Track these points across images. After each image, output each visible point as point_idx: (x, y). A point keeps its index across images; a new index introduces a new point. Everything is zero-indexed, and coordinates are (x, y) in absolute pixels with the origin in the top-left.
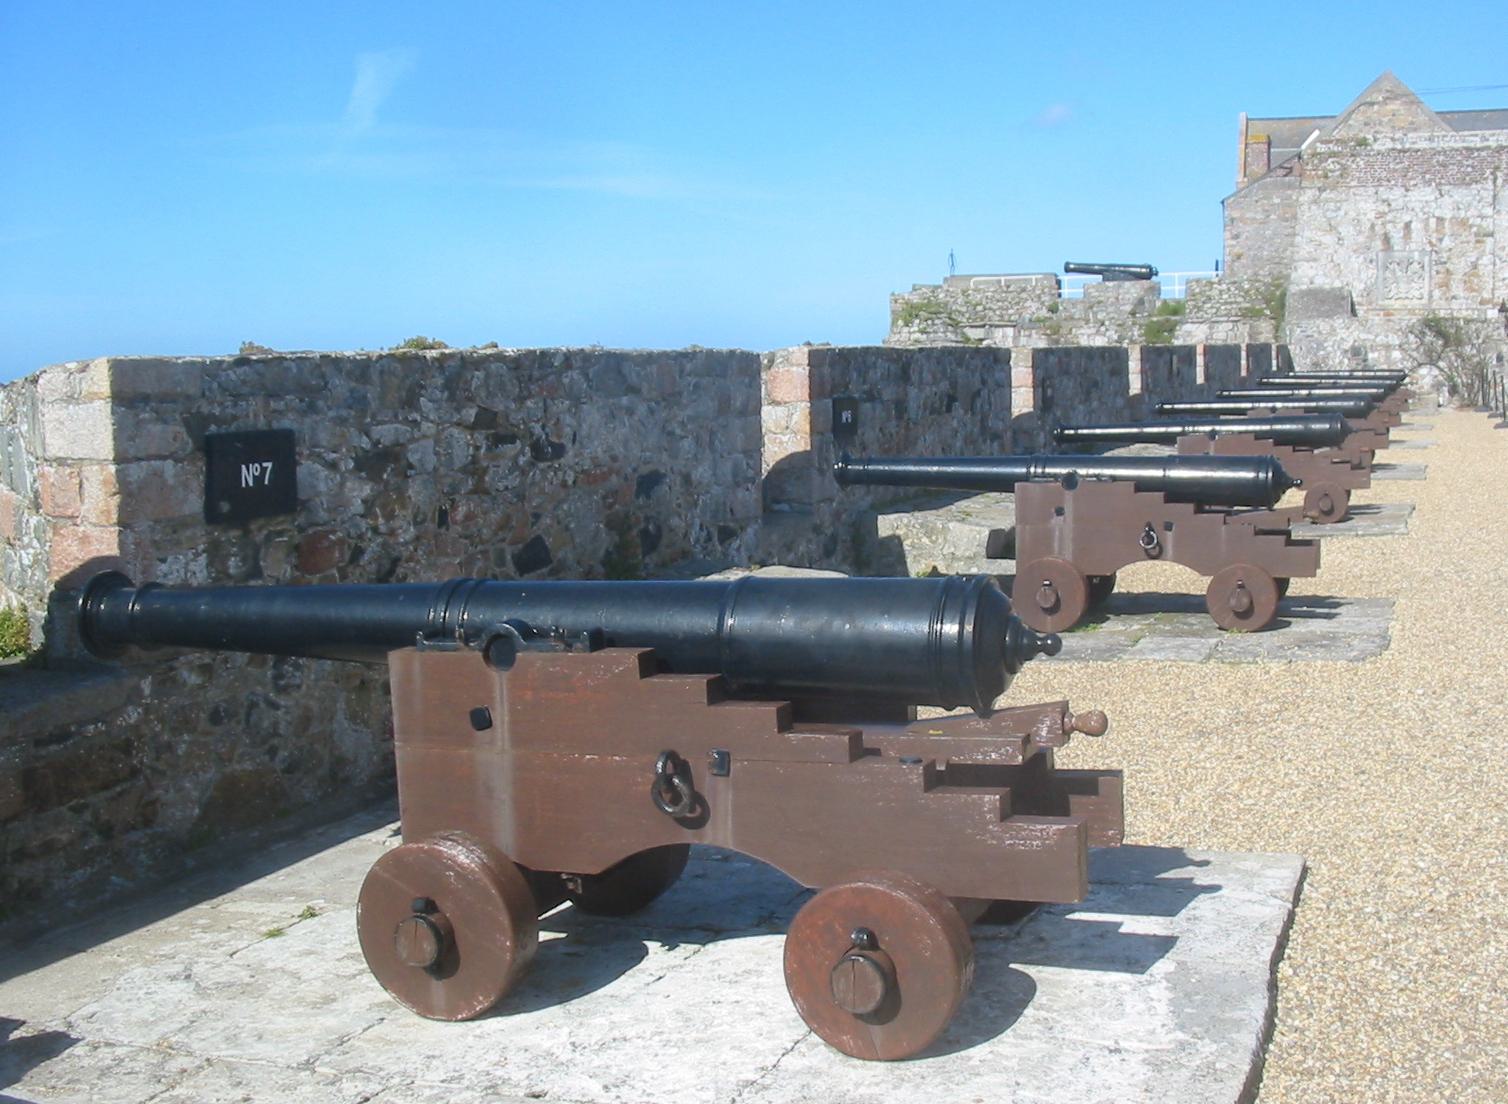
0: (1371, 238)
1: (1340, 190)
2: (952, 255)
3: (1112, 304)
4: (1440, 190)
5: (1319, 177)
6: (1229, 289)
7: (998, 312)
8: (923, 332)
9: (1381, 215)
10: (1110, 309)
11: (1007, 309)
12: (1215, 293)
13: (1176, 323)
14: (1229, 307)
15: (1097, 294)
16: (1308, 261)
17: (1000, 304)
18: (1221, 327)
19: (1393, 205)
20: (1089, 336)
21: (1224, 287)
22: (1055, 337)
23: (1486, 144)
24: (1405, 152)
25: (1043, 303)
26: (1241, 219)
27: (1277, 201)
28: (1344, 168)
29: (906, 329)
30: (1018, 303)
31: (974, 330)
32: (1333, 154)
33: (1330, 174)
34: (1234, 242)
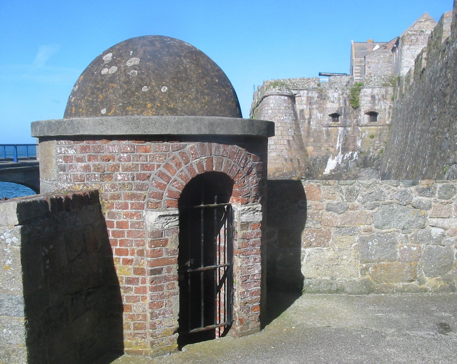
2: (254, 86)
3: (339, 83)
6: (377, 78)
7: (301, 86)
8: (279, 90)
10: (339, 84)
11: (304, 85)
12: (373, 79)
13: (361, 88)
14: (378, 83)
15: (334, 80)
16: (406, 67)
18: (376, 89)
20: (332, 93)
21: (376, 77)
25: (316, 83)
26: (371, 62)
27: (382, 56)
28: (417, 39)
29: (274, 89)
30: (308, 83)
31: (294, 91)
32: (413, 35)
34: (369, 69)
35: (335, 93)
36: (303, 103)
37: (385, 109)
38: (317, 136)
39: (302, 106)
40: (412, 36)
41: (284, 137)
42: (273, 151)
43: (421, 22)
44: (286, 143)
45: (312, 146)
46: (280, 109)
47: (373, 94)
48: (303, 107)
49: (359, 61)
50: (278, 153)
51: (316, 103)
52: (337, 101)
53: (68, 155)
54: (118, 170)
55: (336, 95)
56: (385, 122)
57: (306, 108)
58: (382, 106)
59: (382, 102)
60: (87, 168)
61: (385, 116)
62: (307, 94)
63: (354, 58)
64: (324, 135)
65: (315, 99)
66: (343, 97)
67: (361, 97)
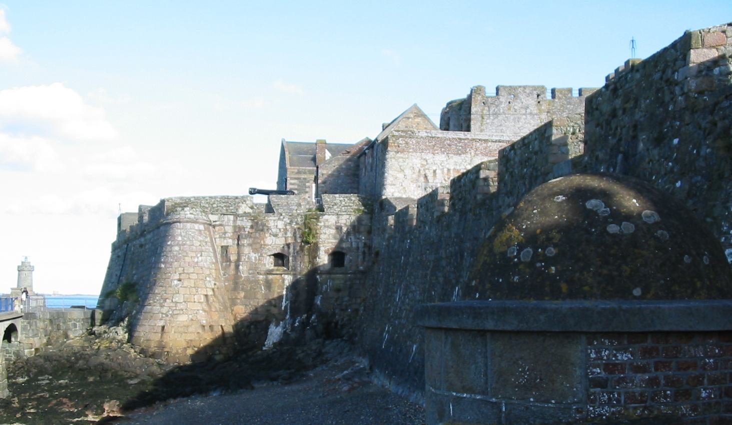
0: (419, 176)
1: (405, 153)
4: (448, 156)
5: (395, 146)
9: (423, 165)
10: (285, 208)
11: (229, 207)
14: (346, 208)
15: (277, 201)
17: (225, 204)
19: (428, 161)
22: (256, 221)
23: (466, 137)
24: (433, 138)
32: (401, 136)
33: (400, 145)
35: (279, 222)
36: (227, 236)
37: (358, 248)
38: (251, 289)
39: (225, 241)
40: (399, 139)
41: (200, 289)
42: (181, 312)
43: (409, 118)
44: (202, 300)
45: (243, 305)
46: (193, 245)
47: (339, 224)
48: (227, 243)
49: (296, 171)
50: (191, 316)
51: (249, 235)
52: (283, 234)
53: (617, 362)
54: (701, 383)
55: (281, 224)
56: (358, 267)
57: (231, 244)
58: (353, 243)
59: (352, 237)
60: (653, 382)
61: (358, 258)
62: (234, 221)
63: (288, 166)
64: (261, 288)
65: (247, 230)
66: (292, 227)
67: (321, 228)
